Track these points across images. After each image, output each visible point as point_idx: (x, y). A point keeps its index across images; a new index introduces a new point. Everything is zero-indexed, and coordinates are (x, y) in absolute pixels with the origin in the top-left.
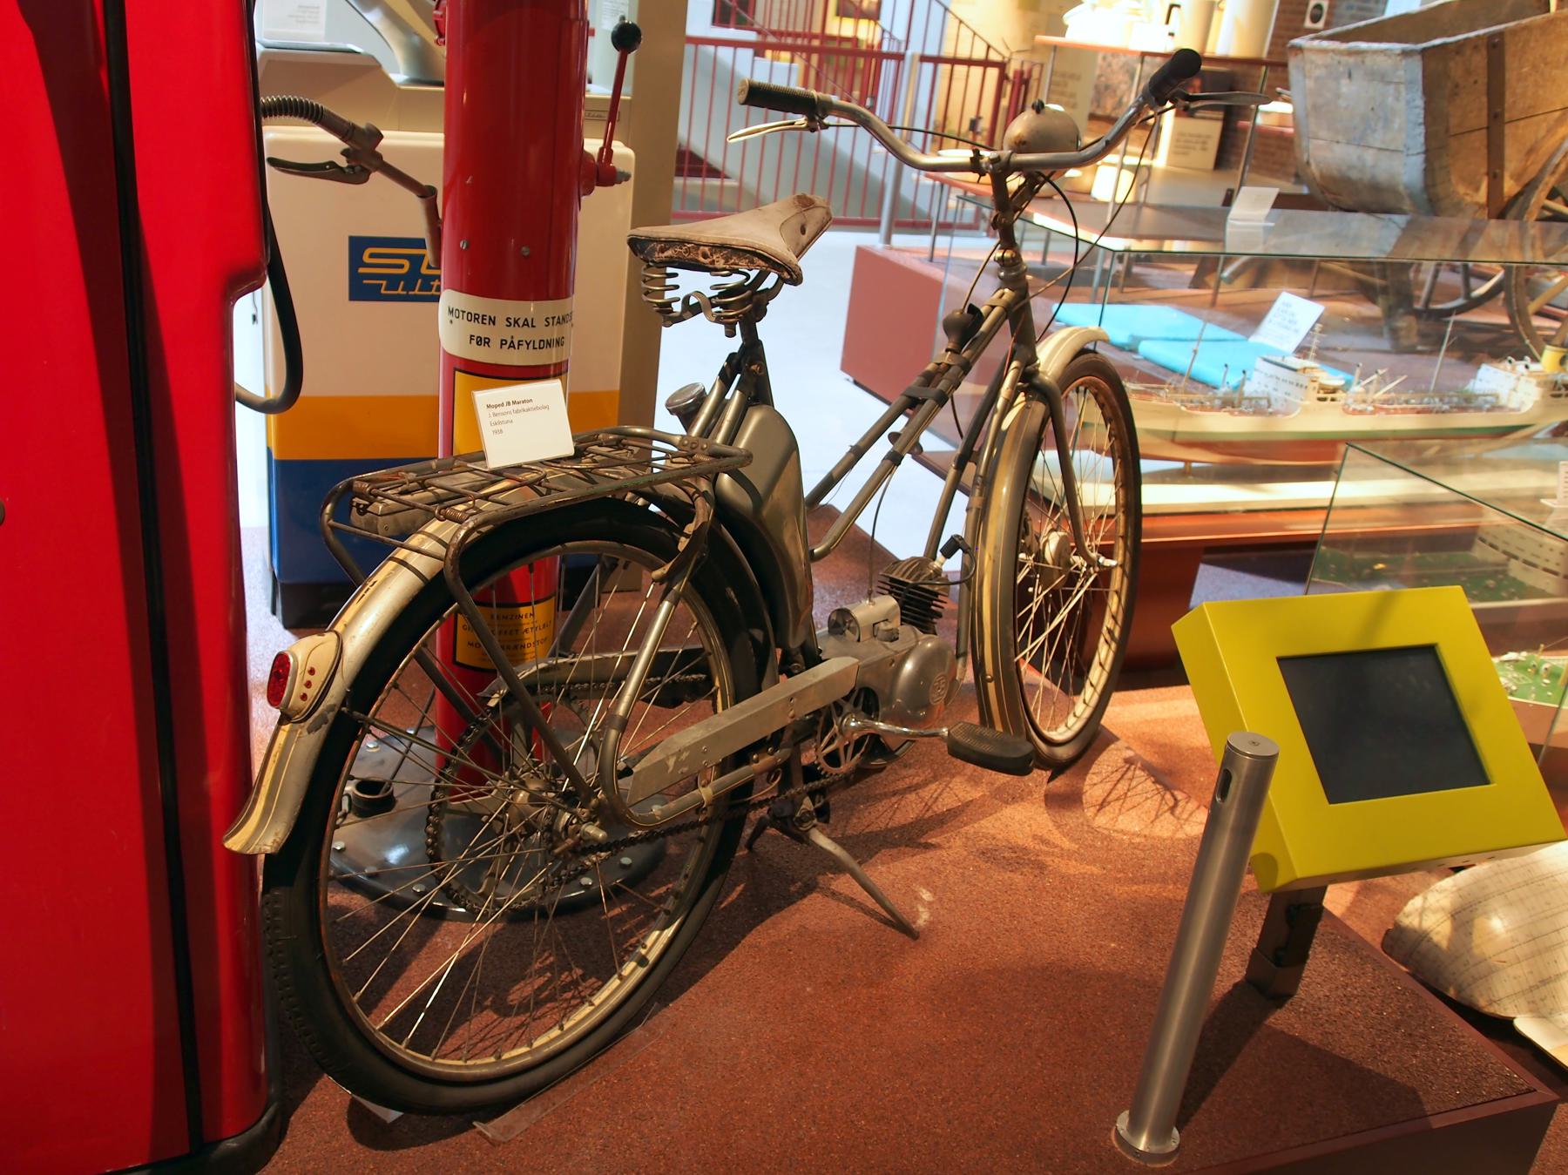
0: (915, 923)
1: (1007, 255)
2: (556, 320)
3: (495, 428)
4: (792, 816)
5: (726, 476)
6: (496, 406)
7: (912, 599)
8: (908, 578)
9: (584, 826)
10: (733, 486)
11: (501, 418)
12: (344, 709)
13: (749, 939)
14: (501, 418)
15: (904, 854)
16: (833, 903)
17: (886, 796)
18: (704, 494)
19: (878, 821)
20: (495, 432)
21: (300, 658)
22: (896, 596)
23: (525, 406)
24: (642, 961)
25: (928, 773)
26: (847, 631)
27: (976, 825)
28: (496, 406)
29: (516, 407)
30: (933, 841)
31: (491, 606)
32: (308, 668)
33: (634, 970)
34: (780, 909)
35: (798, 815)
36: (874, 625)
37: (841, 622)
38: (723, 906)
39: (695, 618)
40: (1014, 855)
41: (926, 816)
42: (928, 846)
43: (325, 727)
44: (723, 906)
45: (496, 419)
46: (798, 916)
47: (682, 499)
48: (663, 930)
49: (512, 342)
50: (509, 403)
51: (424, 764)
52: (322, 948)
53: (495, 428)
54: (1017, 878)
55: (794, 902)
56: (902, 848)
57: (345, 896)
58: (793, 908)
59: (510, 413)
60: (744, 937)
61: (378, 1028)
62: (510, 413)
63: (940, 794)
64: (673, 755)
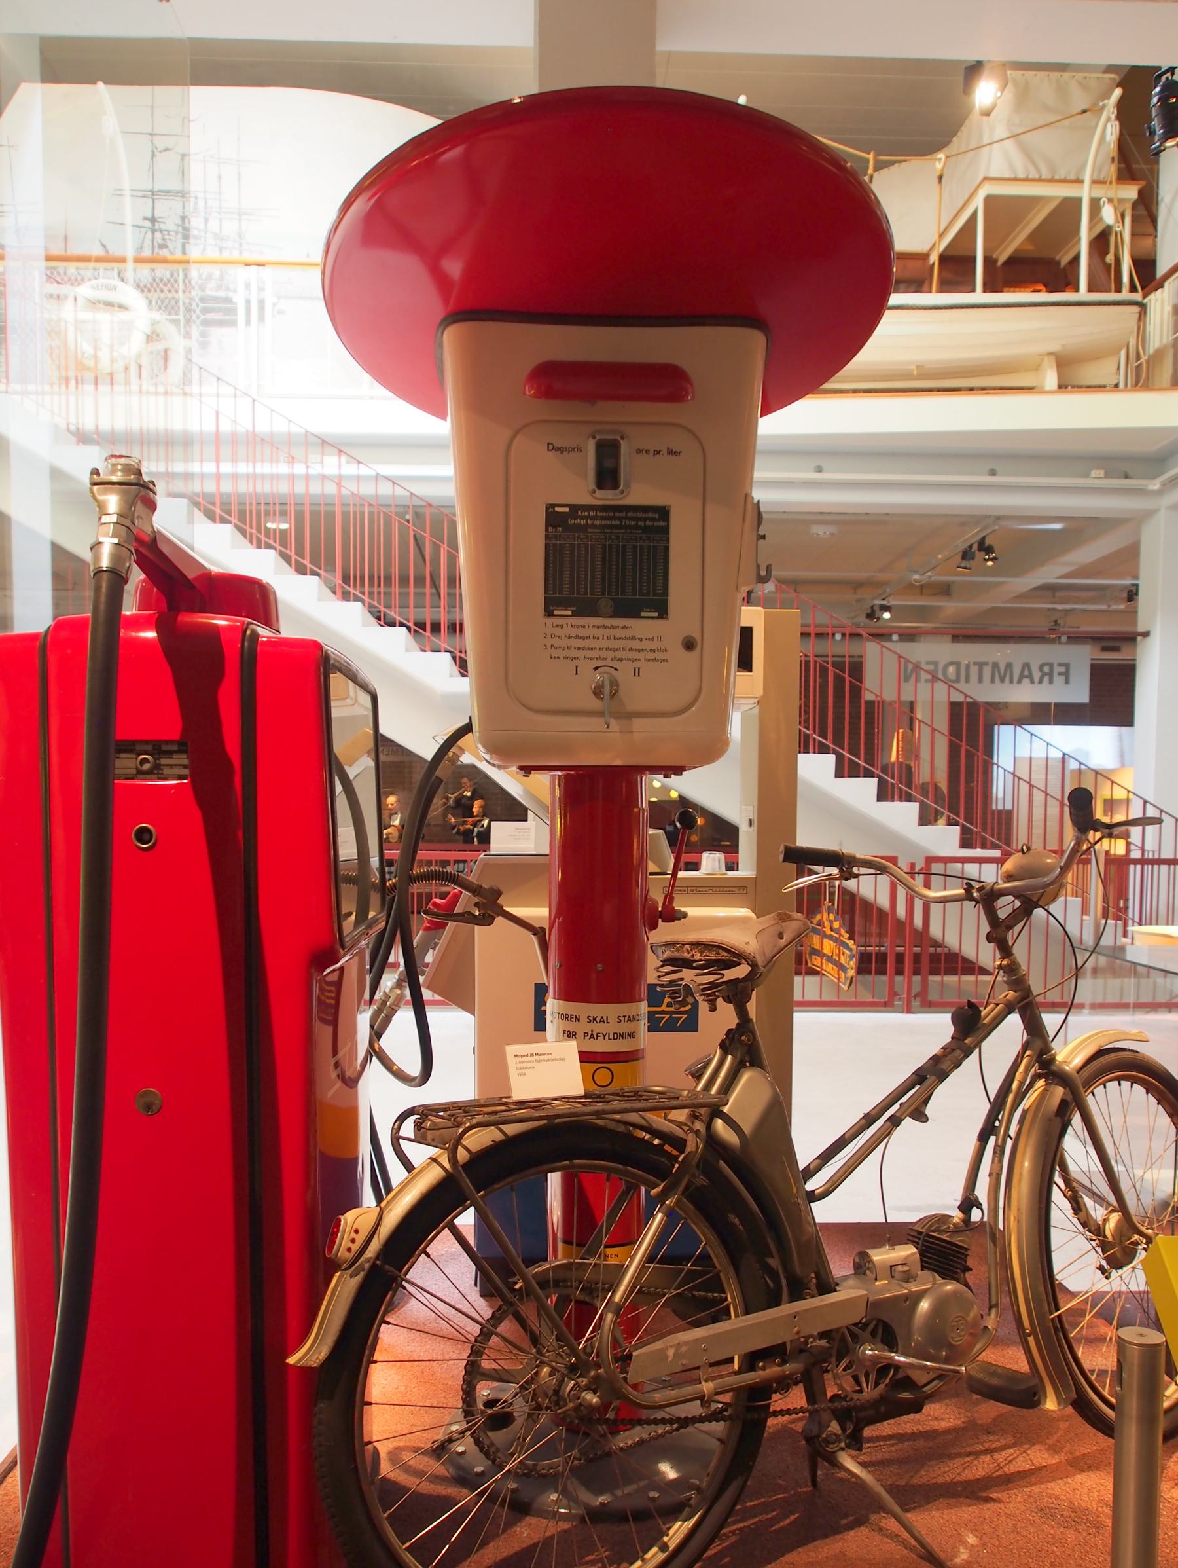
0: (951, 1560)
1: (1005, 962)
2: (626, 1018)
3: (521, 1071)
4: (818, 1436)
5: (720, 1121)
6: (522, 1056)
7: (932, 1248)
8: (922, 1228)
9: (584, 1394)
10: (724, 1126)
11: (525, 1065)
12: (378, 1262)
13: (788, 1557)
14: (525, 1065)
15: (961, 1503)
16: (877, 1537)
17: (959, 1455)
18: (697, 1132)
19: (945, 1475)
20: (520, 1074)
21: (349, 1221)
22: (916, 1245)
23: (546, 1057)
24: (664, 1547)
25: (1010, 1439)
26: (868, 1272)
27: (1042, 1486)
28: (522, 1056)
29: (538, 1058)
30: (994, 1496)
31: (572, 1244)
32: (354, 1228)
33: (656, 1554)
34: (826, 1536)
35: (824, 1435)
36: (891, 1266)
37: (862, 1264)
38: (773, 1528)
39: (703, 1239)
40: (1073, 1515)
41: (994, 1475)
42: (988, 1500)
43: (362, 1274)
44: (773, 1528)
45: (521, 1065)
46: (840, 1544)
47: (677, 1134)
48: (684, 1521)
49: (592, 1034)
50: (532, 1055)
51: (433, 1309)
52: (355, 1461)
53: (521, 1071)
54: (1071, 1535)
55: (842, 1532)
56: (961, 1499)
57: (456, 1489)
58: (838, 1537)
59: (533, 1061)
60: (783, 1555)
61: (404, 1547)
62: (533, 1061)
63: (1014, 1459)
64: (671, 1347)
